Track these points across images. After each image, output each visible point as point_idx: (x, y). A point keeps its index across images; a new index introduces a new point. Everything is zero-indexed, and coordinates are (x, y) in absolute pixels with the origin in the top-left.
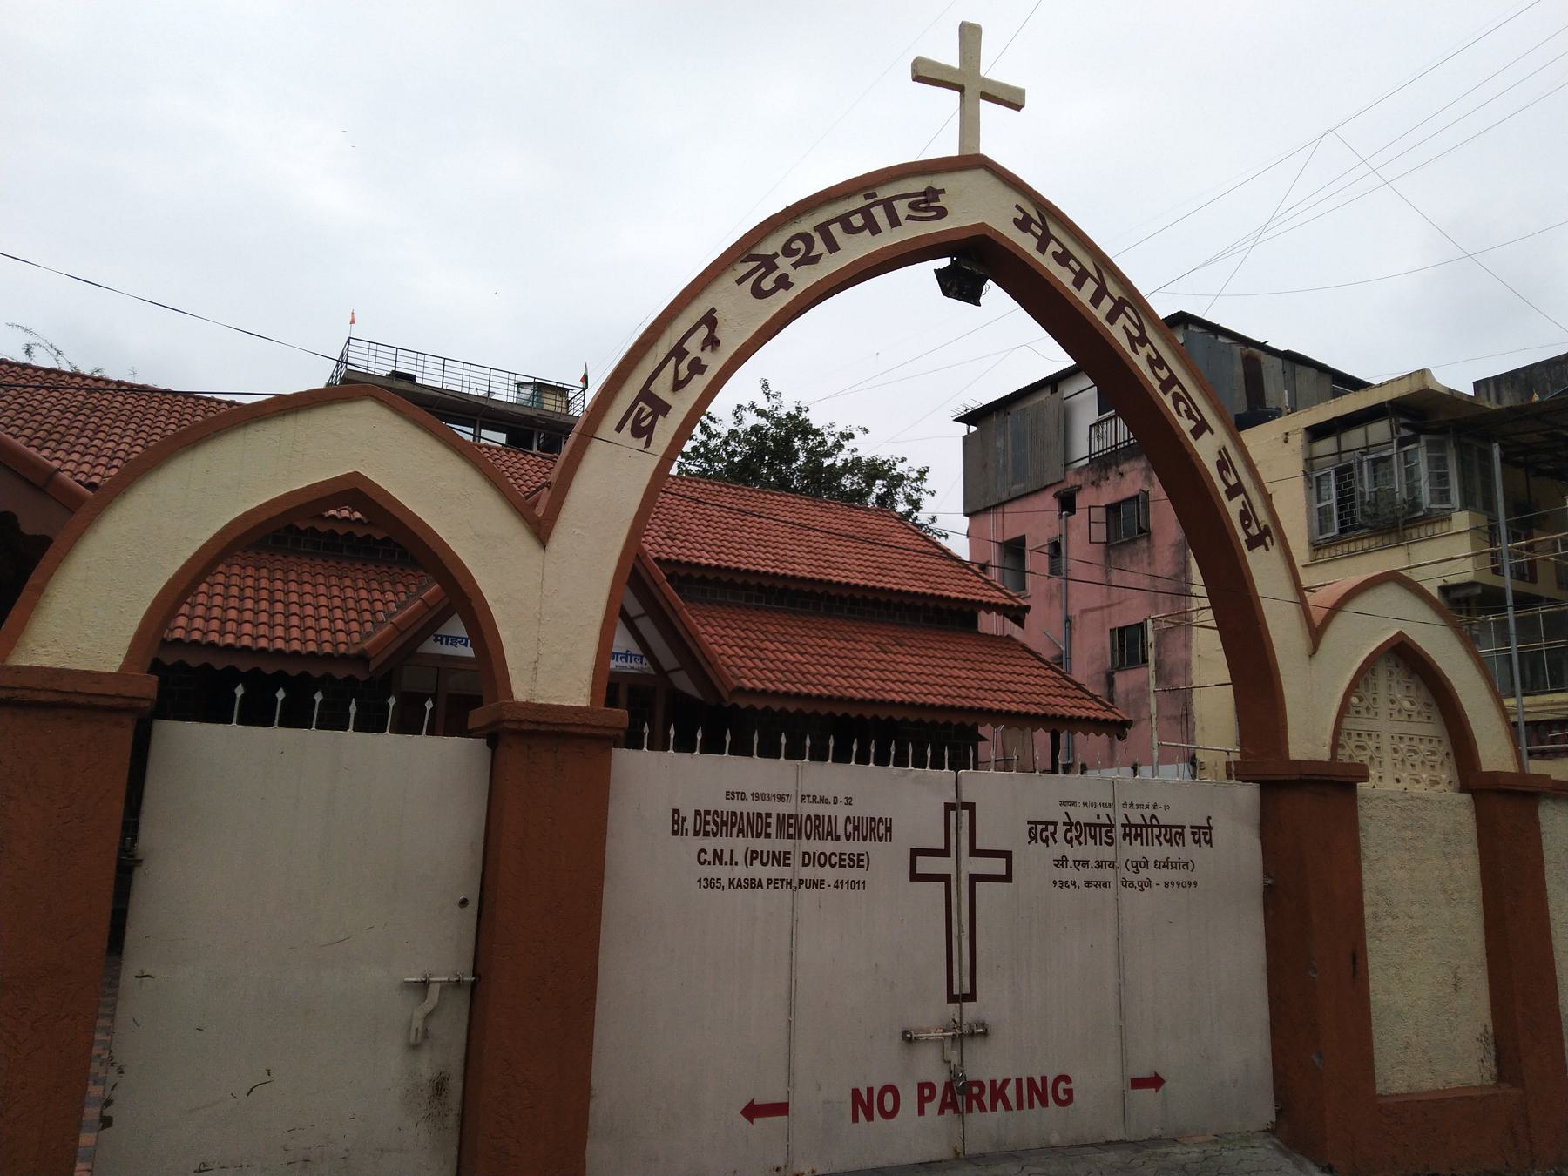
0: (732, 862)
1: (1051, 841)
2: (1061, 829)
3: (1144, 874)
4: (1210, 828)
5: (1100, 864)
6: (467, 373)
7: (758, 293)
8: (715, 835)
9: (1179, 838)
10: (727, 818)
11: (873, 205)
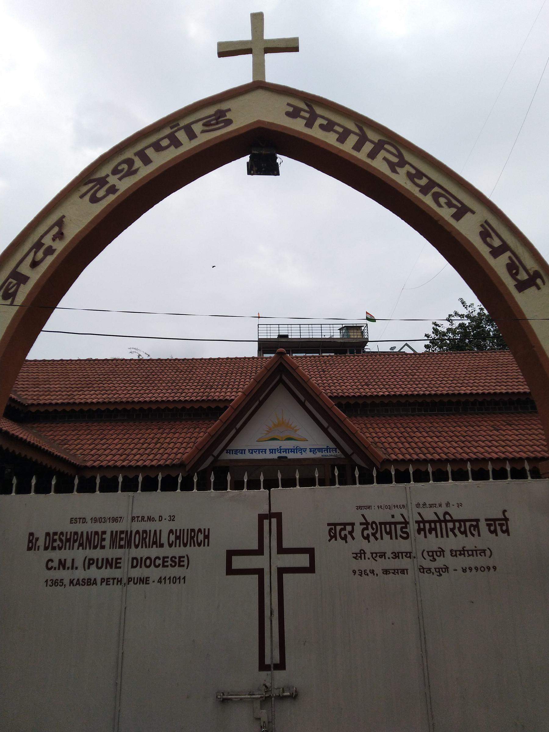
0: (73, 567)
1: (349, 537)
2: (358, 529)
3: (440, 562)
4: (506, 519)
5: (396, 555)
6: (310, 329)
7: (94, 200)
8: (60, 549)
9: (474, 530)
10: (95, 537)
11: (176, 131)
